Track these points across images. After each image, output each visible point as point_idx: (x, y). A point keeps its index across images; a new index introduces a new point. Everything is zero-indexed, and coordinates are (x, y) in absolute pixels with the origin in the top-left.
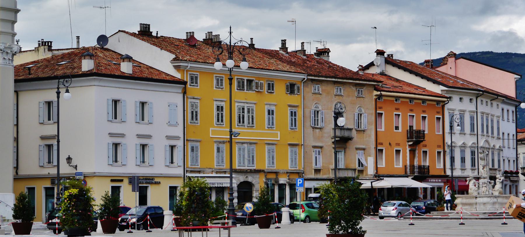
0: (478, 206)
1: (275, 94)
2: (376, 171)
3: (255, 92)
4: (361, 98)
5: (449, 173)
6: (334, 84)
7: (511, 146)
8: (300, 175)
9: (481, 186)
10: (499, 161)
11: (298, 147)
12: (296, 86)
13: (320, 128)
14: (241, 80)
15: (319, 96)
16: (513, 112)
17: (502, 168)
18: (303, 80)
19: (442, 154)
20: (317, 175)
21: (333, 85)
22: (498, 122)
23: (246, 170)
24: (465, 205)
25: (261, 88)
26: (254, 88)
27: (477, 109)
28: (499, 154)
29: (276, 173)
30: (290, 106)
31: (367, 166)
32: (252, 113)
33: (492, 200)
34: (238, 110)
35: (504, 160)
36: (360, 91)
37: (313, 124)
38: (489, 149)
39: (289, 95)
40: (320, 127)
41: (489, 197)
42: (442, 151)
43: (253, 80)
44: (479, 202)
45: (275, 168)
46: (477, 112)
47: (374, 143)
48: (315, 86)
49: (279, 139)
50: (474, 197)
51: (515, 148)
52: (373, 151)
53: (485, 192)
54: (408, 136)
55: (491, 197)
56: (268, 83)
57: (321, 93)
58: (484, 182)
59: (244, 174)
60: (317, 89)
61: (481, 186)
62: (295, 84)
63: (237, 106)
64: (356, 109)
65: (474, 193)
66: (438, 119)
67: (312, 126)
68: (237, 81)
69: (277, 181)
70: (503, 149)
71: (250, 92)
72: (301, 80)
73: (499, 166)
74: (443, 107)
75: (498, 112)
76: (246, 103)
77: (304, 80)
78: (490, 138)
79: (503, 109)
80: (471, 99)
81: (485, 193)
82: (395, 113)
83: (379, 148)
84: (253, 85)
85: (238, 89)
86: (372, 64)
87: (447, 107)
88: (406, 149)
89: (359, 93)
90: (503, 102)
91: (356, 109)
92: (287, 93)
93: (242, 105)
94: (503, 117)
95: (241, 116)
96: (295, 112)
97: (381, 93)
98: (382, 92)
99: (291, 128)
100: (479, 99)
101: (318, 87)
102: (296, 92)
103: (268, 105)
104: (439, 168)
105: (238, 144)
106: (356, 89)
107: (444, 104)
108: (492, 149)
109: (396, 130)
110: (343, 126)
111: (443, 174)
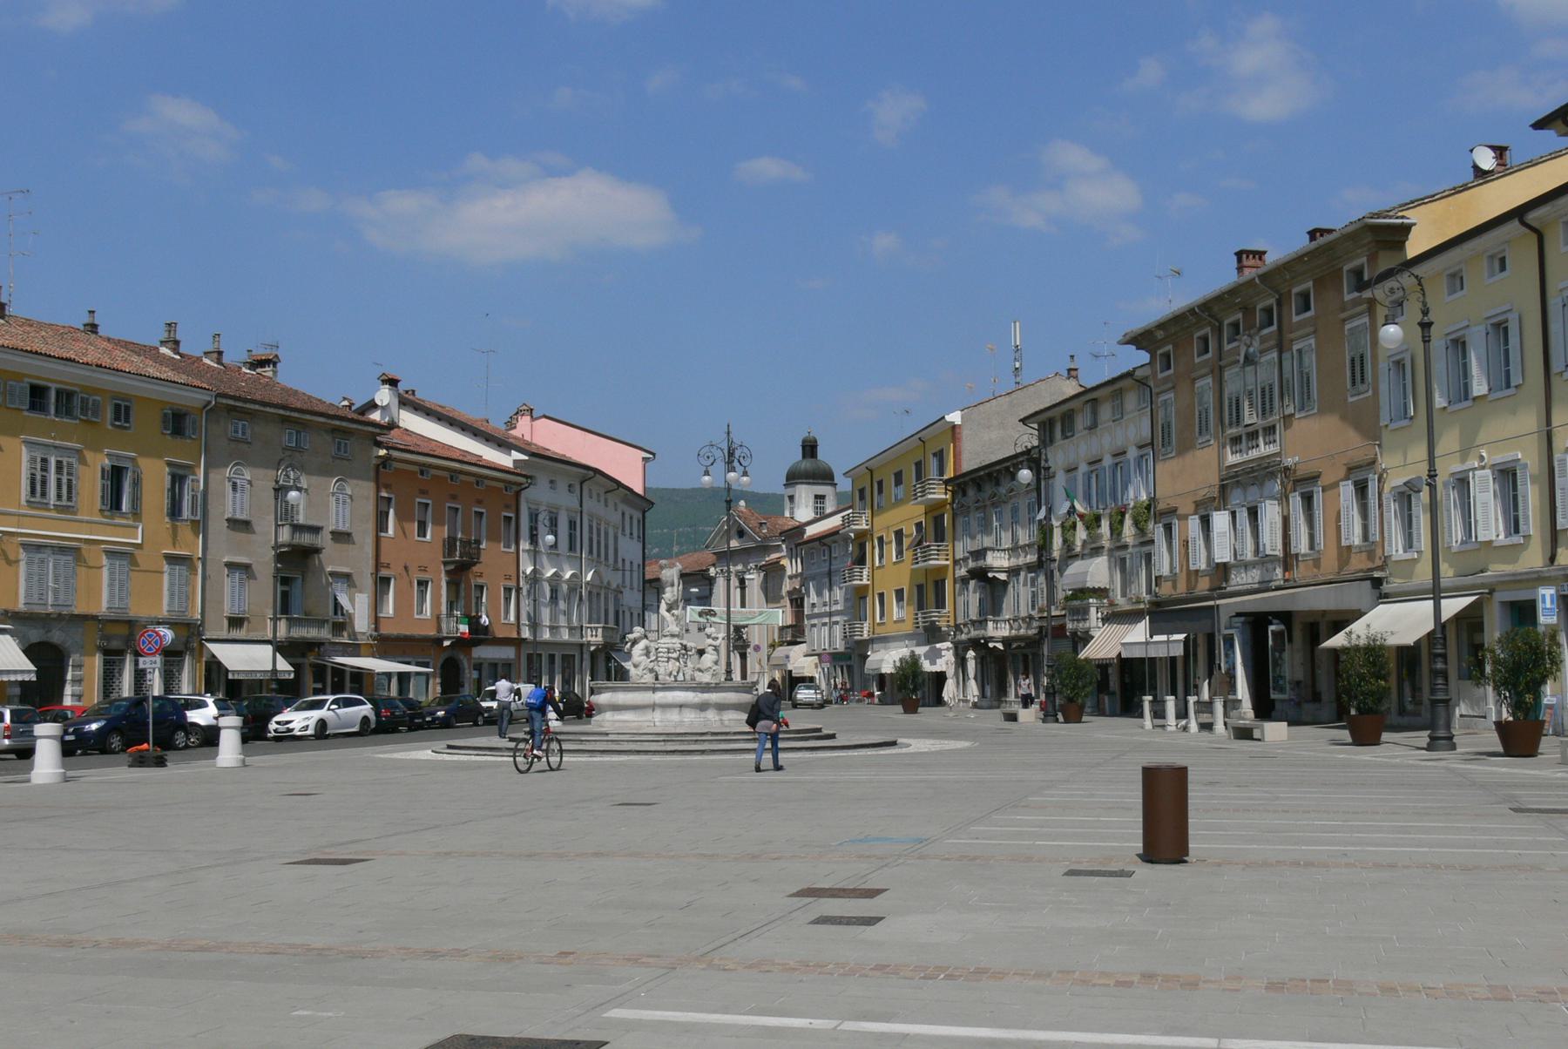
3: (78, 421)
4: (345, 461)
5: (526, 633)
7: (635, 585)
8: (192, 630)
12: (188, 417)
15: (245, 447)
16: (639, 521)
18: (205, 407)
22: (616, 538)
25: (96, 413)
26: (77, 412)
27: (581, 506)
31: (354, 614)
32: (68, 474)
35: (624, 612)
36: (343, 445)
38: (601, 587)
39: (169, 438)
43: (75, 392)
46: (581, 512)
47: (371, 562)
48: (237, 424)
49: (139, 541)
52: (368, 582)
57: (249, 440)
62: (185, 415)
66: (508, 519)
70: (623, 589)
71: (65, 420)
74: (518, 494)
75: (615, 518)
76: (52, 448)
77: (209, 408)
78: (603, 566)
79: (623, 514)
82: (418, 500)
83: (384, 573)
84: (75, 404)
87: (524, 494)
88: (441, 580)
89: (339, 449)
92: (165, 432)
94: (623, 530)
95: (38, 478)
98: (391, 452)
101: (244, 425)
106: (334, 438)
107: (519, 488)
108: (606, 588)
109: (418, 536)
111: (515, 635)
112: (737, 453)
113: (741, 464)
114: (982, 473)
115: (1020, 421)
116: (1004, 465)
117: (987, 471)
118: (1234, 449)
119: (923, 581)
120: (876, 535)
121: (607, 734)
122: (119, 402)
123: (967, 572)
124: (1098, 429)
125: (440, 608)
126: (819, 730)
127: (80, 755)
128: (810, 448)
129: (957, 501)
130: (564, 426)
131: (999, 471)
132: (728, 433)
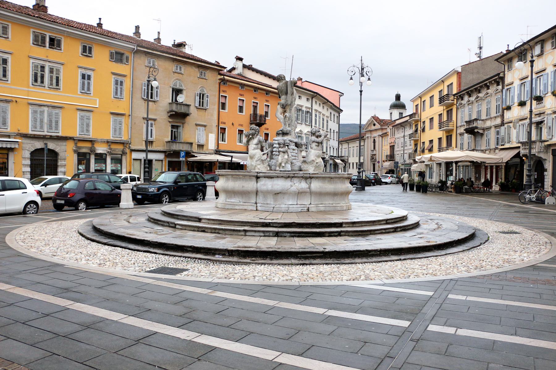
0: (260, 200)
1: (93, 58)
2: (217, 147)
6: (173, 62)
9: (276, 151)
10: (327, 147)
11: (124, 117)
13: (154, 101)
14: (39, 34)
16: (337, 117)
17: (328, 153)
20: (150, 147)
21: (172, 62)
23: (43, 136)
24: (233, 195)
27: (312, 106)
28: (327, 143)
29: (92, 141)
30: (114, 74)
32: (56, 74)
33: (297, 184)
34: (33, 68)
37: (144, 96)
40: (154, 100)
41: (289, 177)
44: (264, 188)
45: (91, 135)
47: (216, 121)
50: (253, 176)
53: (283, 165)
54: (251, 119)
55: (293, 177)
56: (84, 46)
58: (282, 142)
59: (42, 140)
60: (152, 63)
61: (276, 151)
63: (33, 63)
64: (198, 89)
65: (259, 167)
67: (144, 97)
68: (33, 34)
69: (93, 150)
72: (131, 50)
73: (327, 151)
75: (328, 114)
79: (331, 113)
81: (283, 167)
83: (222, 126)
85: (35, 43)
86: (234, 69)
89: (201, 75)
90: (331, 108)
91: (198, 89)
93: (42, 63)
95: (39, 75)
96: (121, 82)
97: (224, 78)
99: (115, 96)
100: (314, 100)
102: (125, 61)
103: (83, 69)
105: (32, 105)
110: (182, 102)
112: (365, 70)
113: (367, 75)
118: (537, 103)
119: (442, 136)
120: (422, 121)
121: (199, 220)
122: (86, 45)
123: (464, 130)
124: (544, 55)
126: (404, 218)
128: (398, 97)
130: (332, 102)
132: (361, 60)
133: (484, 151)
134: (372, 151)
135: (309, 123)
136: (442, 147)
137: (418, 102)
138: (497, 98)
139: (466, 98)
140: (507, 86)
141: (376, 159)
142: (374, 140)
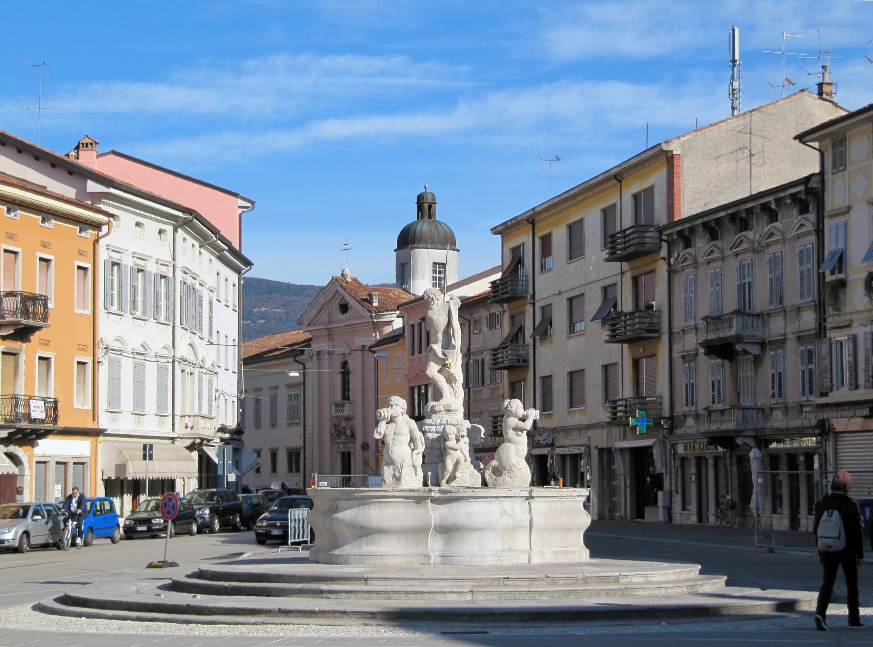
19: (89, 367)
27: (174, 259)
42: (89, 360)
51: (235, 373)
72: (840, 445)
80: (161, 232)
104: (79, 407)
114: (722, 214)
115: (795, 138)
116: (762, 201)
117: (730, 212)
125: (26, 367)
127: (41, 430)
129: (676, 255)
131: (750, 211)
133: (768, 411)
134: (337, 405)
135: (167, 318)
136: (620, 397)
137: (524, 238)
138: (801, 252)
139: (701, 244)
140: (831, 217)
141: (353, 436)
142: (345, 364)
